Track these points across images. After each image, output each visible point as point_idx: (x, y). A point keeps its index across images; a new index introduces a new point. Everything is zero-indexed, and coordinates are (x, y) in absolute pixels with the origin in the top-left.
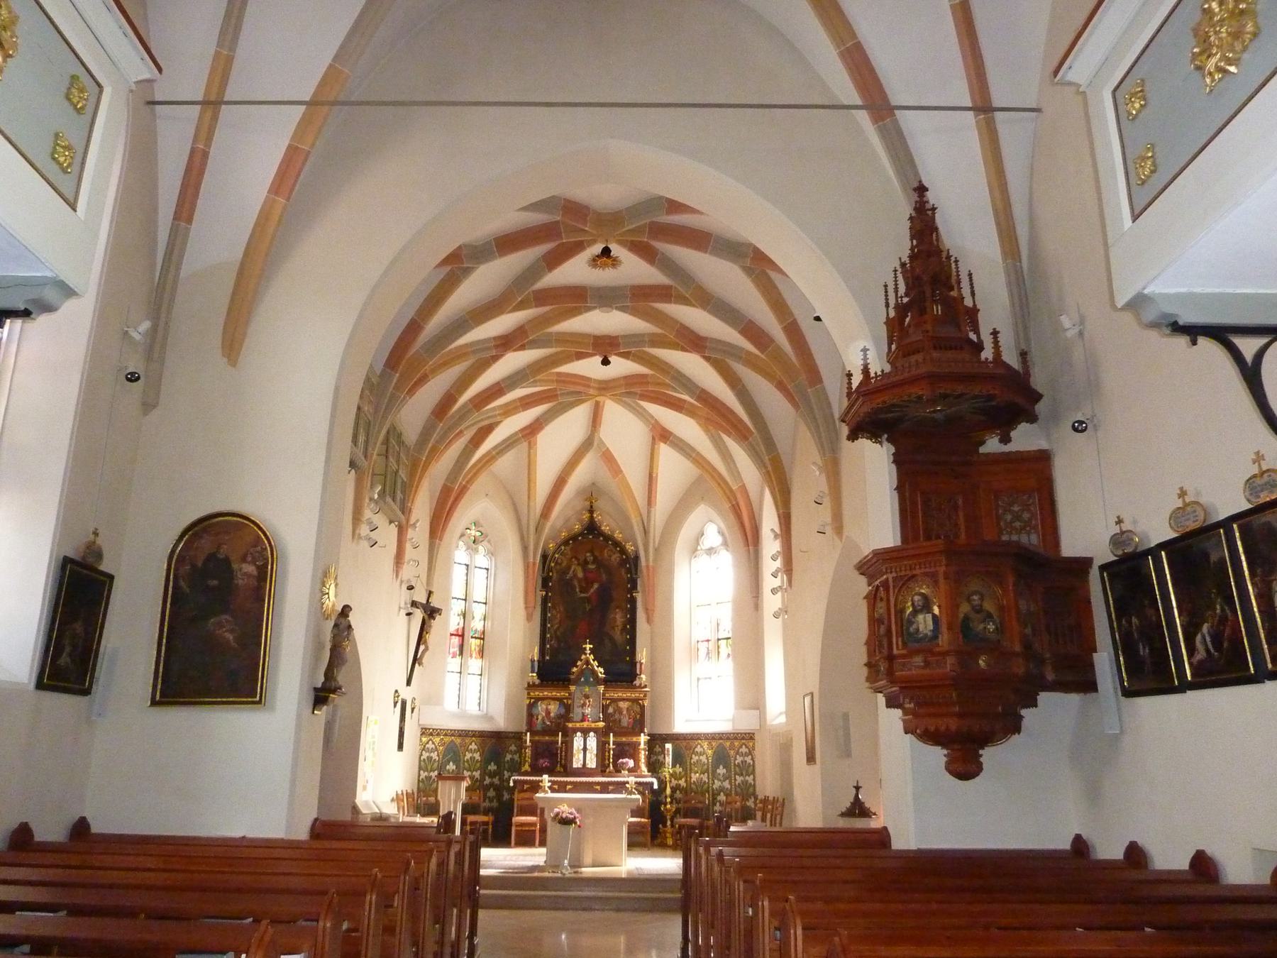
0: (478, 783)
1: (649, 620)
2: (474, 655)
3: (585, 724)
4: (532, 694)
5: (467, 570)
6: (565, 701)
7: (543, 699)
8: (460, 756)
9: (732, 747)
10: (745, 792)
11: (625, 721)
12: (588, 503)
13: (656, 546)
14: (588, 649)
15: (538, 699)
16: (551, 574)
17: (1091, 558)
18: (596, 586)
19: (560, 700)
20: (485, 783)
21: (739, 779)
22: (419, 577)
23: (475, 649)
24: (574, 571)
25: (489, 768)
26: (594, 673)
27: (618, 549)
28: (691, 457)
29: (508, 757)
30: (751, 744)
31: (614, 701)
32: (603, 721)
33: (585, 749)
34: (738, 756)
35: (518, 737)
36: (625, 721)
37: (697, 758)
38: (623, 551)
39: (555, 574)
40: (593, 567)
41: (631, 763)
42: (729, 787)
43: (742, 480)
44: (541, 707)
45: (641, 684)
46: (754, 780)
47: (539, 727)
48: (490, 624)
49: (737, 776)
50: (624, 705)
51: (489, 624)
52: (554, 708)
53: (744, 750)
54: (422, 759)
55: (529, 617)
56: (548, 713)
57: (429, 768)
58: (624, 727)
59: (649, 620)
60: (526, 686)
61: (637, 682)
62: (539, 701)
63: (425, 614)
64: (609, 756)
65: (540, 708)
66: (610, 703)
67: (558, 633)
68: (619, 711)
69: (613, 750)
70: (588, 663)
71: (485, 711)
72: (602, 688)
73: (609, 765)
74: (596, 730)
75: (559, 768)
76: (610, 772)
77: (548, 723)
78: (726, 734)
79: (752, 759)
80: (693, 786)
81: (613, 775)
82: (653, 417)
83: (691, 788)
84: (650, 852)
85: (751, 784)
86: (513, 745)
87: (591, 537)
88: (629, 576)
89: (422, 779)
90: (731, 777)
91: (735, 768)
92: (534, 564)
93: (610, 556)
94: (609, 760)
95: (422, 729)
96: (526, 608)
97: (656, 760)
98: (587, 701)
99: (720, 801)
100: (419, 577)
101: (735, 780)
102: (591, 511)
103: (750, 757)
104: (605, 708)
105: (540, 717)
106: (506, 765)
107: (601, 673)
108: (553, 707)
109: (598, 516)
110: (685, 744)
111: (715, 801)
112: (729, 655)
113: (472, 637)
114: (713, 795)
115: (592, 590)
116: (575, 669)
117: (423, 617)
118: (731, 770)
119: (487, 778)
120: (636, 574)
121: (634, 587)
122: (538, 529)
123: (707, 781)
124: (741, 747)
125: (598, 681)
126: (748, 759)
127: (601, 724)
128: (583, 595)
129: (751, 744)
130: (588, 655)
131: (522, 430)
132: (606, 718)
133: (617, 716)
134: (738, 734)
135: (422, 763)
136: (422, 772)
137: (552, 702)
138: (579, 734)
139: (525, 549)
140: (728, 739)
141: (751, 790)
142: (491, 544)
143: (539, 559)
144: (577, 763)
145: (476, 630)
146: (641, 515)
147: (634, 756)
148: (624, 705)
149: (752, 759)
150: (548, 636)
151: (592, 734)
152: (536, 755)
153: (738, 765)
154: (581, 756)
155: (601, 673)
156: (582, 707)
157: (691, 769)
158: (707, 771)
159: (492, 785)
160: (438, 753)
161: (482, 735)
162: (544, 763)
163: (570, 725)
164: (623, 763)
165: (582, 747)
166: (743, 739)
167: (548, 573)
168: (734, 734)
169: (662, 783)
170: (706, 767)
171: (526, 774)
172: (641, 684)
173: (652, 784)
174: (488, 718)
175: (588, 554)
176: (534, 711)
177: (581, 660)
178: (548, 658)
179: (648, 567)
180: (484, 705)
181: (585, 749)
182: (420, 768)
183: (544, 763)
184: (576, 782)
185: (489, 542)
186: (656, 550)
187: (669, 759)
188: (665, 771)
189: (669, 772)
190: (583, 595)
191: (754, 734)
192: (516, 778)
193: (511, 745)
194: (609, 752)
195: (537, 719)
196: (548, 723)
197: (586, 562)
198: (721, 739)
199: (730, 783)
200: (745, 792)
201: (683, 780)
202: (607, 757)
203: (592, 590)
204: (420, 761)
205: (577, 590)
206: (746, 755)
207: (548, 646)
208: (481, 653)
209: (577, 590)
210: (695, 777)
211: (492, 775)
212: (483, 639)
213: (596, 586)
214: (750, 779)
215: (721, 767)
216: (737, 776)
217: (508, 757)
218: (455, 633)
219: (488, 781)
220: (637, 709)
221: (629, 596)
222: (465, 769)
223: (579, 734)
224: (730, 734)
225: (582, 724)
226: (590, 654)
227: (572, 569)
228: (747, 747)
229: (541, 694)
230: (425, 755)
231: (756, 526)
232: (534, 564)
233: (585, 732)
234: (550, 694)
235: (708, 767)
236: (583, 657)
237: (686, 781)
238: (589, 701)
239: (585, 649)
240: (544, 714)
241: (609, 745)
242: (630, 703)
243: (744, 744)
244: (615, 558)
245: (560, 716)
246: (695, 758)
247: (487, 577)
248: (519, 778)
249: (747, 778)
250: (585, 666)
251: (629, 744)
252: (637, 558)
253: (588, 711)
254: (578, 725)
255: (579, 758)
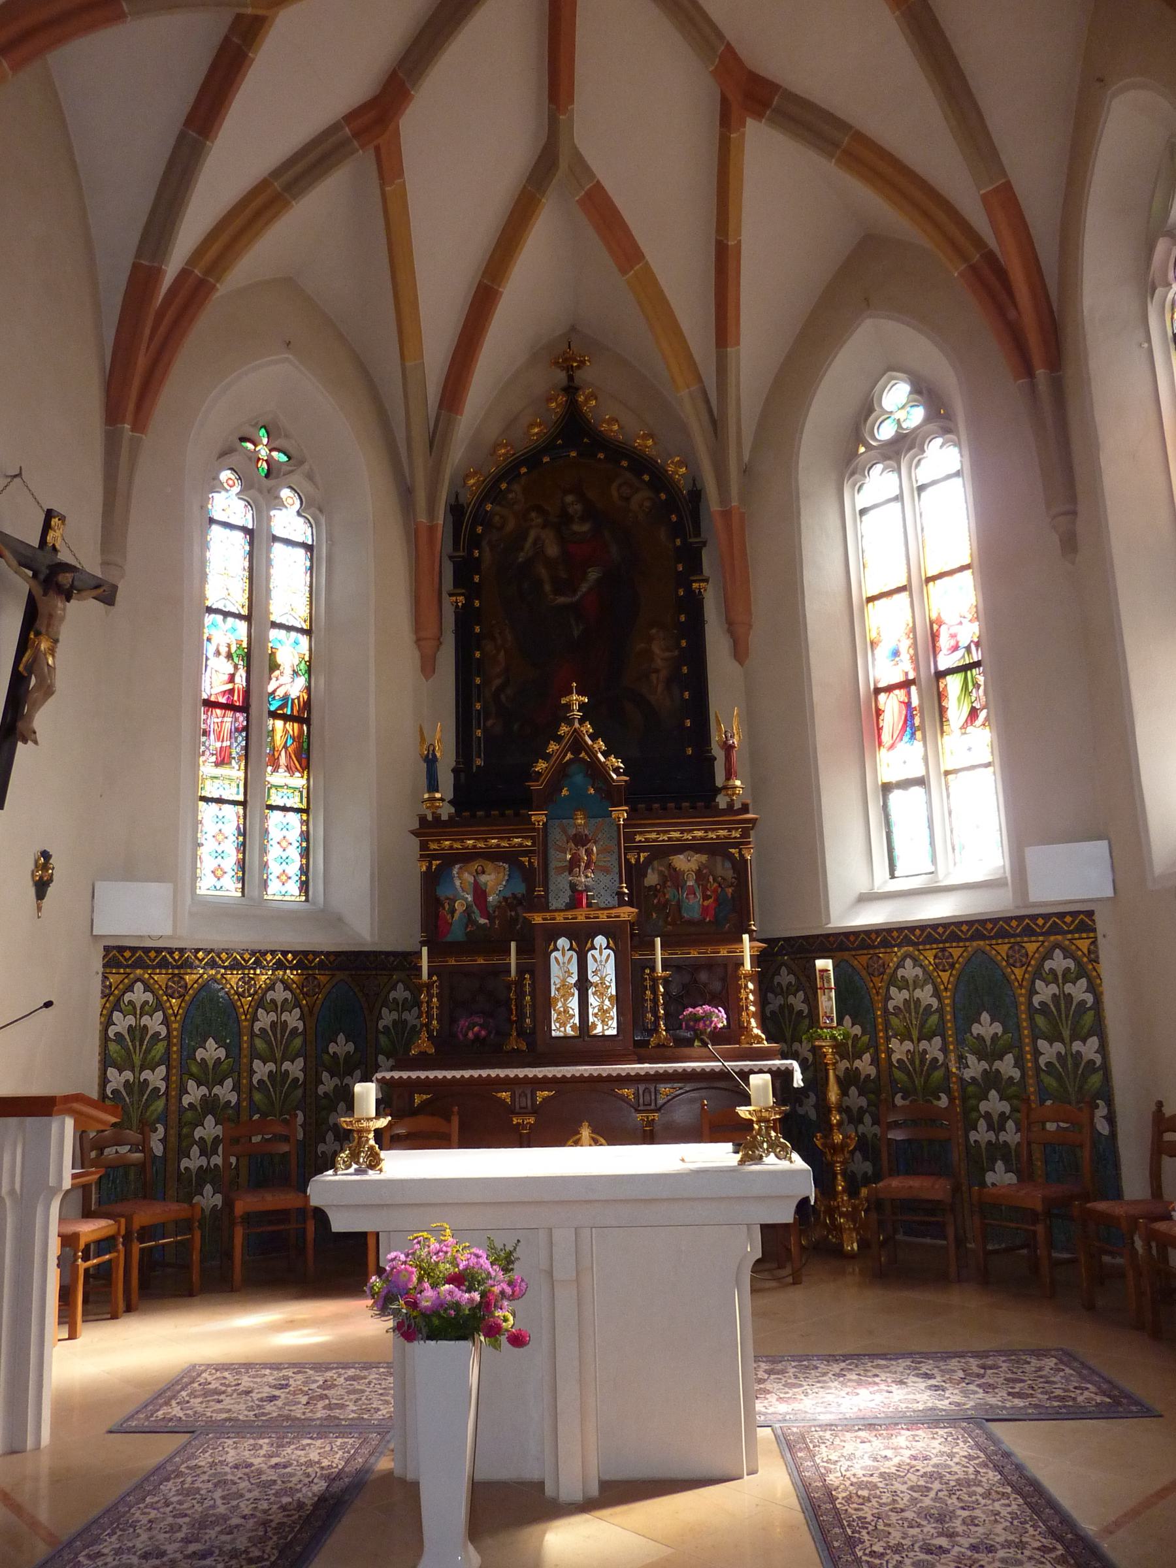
0: (299, 1092)
1: (740, 652)
2: (283, 760)
3: (581, 916)
4: (433, 846)
5: (251, 543)
6: (525, 859)
7: (466, 858)
8: (238, 1021)
9: (1018, 957)
10: (919, 1082)
11: (694, 905)
12: (561, 376)
13: (746, 459)
14: (576, 707)
15: (451, 859)
16: (476, 553)
17: (363, 1235)
18: (593, 575)
19: (509, 857)
20: (321, 1090)
21: (1049, 1051)
22: (19, 475)
23: (285, 747)
24: (535, 543)
25: (332, 1048)
26: (596, 772)
27: (646, 478)
28: (836, 145)
29: (388, 1018)
30: (1084, 945)
31: (662, 852)
32: (630, 904)
33: (583, 985)
34: (1039, 984)
35: (405, 961)
36: (694, 905)
37: (905, 994)
38: (660, 480)
39: (487, 555)
40: (585, 528)
41: (720, 1018)
42: (1016, 1074)
43: (1004, 173)
44: (462, 879)
45: (731, 805)
46: (1103, 1049)
47: (457, 933)
48: (322, 681)
49: (1040, 1042)
50: (685, 863)
51: (320, 683)
52: (495, 880)
53: (1059, 962)
54: (111, 1034)
55: (428, 666)
56: (480, 893)
57: (137, 1059)
58: (691, 923)
59: (740, 652)
60: (416, 825)
61: (722, 801)
62: (457, 862)
63: (34, 583)
64: (655, 1001)
65: (458, 883)
66: (648, 861)
67: (503, 697)
68: (674, 877)
69: (666, 983)
70: (577, 745)
71: (321, 899)
72: (621, 814)
73: (657, 1025)
74: (611, 931)
75: (514, 1043)
76: (658, 1046)
77: (482, 921)
78: (995, 921)
79: (1093, 988)
80: (898, 1074)
81: (668, 1052)
82: (720, 35)
83: (893, 1081)
84: (796, 1295)
85: (935, 1060)
86: (400, 986)
87: (573, 454)
88: (678, 542)
89: (260, 1081)
90: (1021, 1049)
91: (1031, 1019)
92: (432, 529)
93: (627, 499)
94: (655, 1012)
95: (107, 949)
96: (418, 641)
97: (781, 1007)
98: (582, 852)
99: (988, 1116)
100: (19, 475)
101: (1037, 1053)
102: (571, 389)
103: (1083, 982)
104: (634, 874)
105: (459, 906)
106: (383, 1040)
107: (616, 770)
108: (493, 876)
109: (587, 399)
110: (864, 960)
111: (974, 1115)
112: (973, 713)
113: (274, 715)
114: (965, 1099)
115: (584, 588)
116: (541, 766)
117: (30, 594)
118: (1018, 1027)
119: (325, 1076)
120: (698, 534)
121: (695, 566)
122: (438, 439)
123: (941, 1058)
124: (1048, 955)
125: (611, 795)
126: (1078, 991)
127: (627, 913)
128: (561, 600)
129: (1084, 945)
130: (577, 725)
131: (350, 117)
132: (638, 896)
133: (670, 893)
134: (1034, 918)
135: (113, 1047)
136: (112, 1072)
137: (489, 866)
138: (563, 942)
139: (406, 493)
140: (1003, 934)
141: (1095, 1080)
142: (315, 484)
143: (442, 516)
144: (562, 1027)
145: (286, 698)
146: (699, 379)
147: (729, 1000)
148: (685, 863)
149: (1093, 988)
150: (478, 706)
151: (600, 940)
152: (453, 1006)
153: (1044, 1008)
154: (574, 1004)
155: (616, 770)
156: (570, 872)
157: (887, 1025)
158: (940, 1031)
159: (210, 1106)
160: (165, 1016)
161: (304, 960)
162: (472, 1028)
163: (538, 919)
164: (696, 1019)
165: (574, 979)
166: (1055, 930)
167: (471, 553)
168: (1020, 918)
169: (815, 1070)
170: (934, 1019)
171: (423, 1062)
172: (731, 805)
173: (789, 1073)
174: (329, 918)
175: (569, 498)
176: (442, 892)
177: (559, 739)
178: (479, 762)
179: (727, 514)
180: (317, 887)
181: (583, 985)
182: (106, 1062)
183: (470, 1028)
184: (564, 1080)
185: (310, 477)
186: (746, 471)
187: (828, 1002)
188: (820, 1038)
189: (833, 1038)
190: (561, 600)
191: (1090, 914)
192: (388, 1075)
193: (394, 988)
194: (654, 990)
195: (453, 911)
196: (482, 921)
197: (566, 517)
198: (978, 936)
199: (1019, 1063)
200: (919, 1082)
201: (867, 1057)
202: (649, 1004)
203: (584, 588)
204: (105, 1039)
205: (547, 588)
206: (1067, 977)
207: (479, 733)
208: (303, 758)
209: (547, 588)
210: (900, 1049)
211: (210, 1075)
212: (307, 721)
213: (593, 575)
214: (1089, 1049)
215: (985, 1017)
216: (1040, 1042)
217: (388, 1018)
218: (223, 700)
219: (195, 1093)
220: (724, 870)
221: (681, 592)
222: (254, 1054)
223: (563, 942)
224: (1008, 920)
225: (569, 914)
226: (581, 721)
227: (530, 540)
228: (1067, 954)
229: (457, 845)
230: (122, 1024)
231: (1053, 320)
232: (432, 529)
233: (582, 940)
234: (481, 845)
235: (942, 1017)
236: (564, 729)
237: (875, 1061)
238: (589, 853)
239: (568, 707)
240: (470, 898)
241: (653, 969)
242: (704, 858)
243: (1057, 945)
244: (641, 500)
245: (511, 903)
246: (898, 997)
247: (311, 568)
248: (396, 1075)
249: (1077, 1046)
250: (569, 756)
251: (710, 965)
252: (697, 495)
253: (584, 879)
254: (560, 918)
255: (566, 1011)
